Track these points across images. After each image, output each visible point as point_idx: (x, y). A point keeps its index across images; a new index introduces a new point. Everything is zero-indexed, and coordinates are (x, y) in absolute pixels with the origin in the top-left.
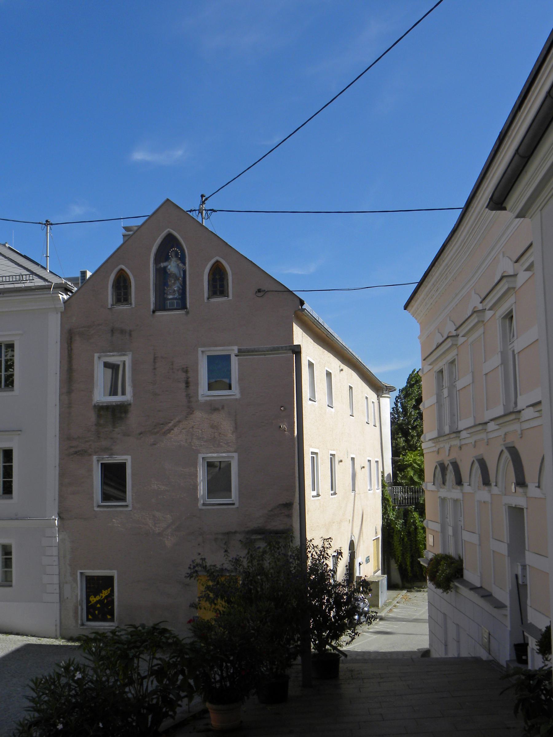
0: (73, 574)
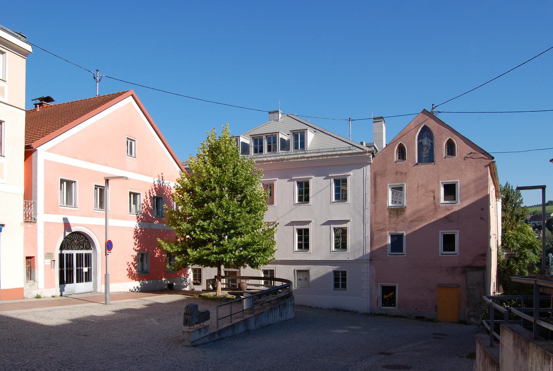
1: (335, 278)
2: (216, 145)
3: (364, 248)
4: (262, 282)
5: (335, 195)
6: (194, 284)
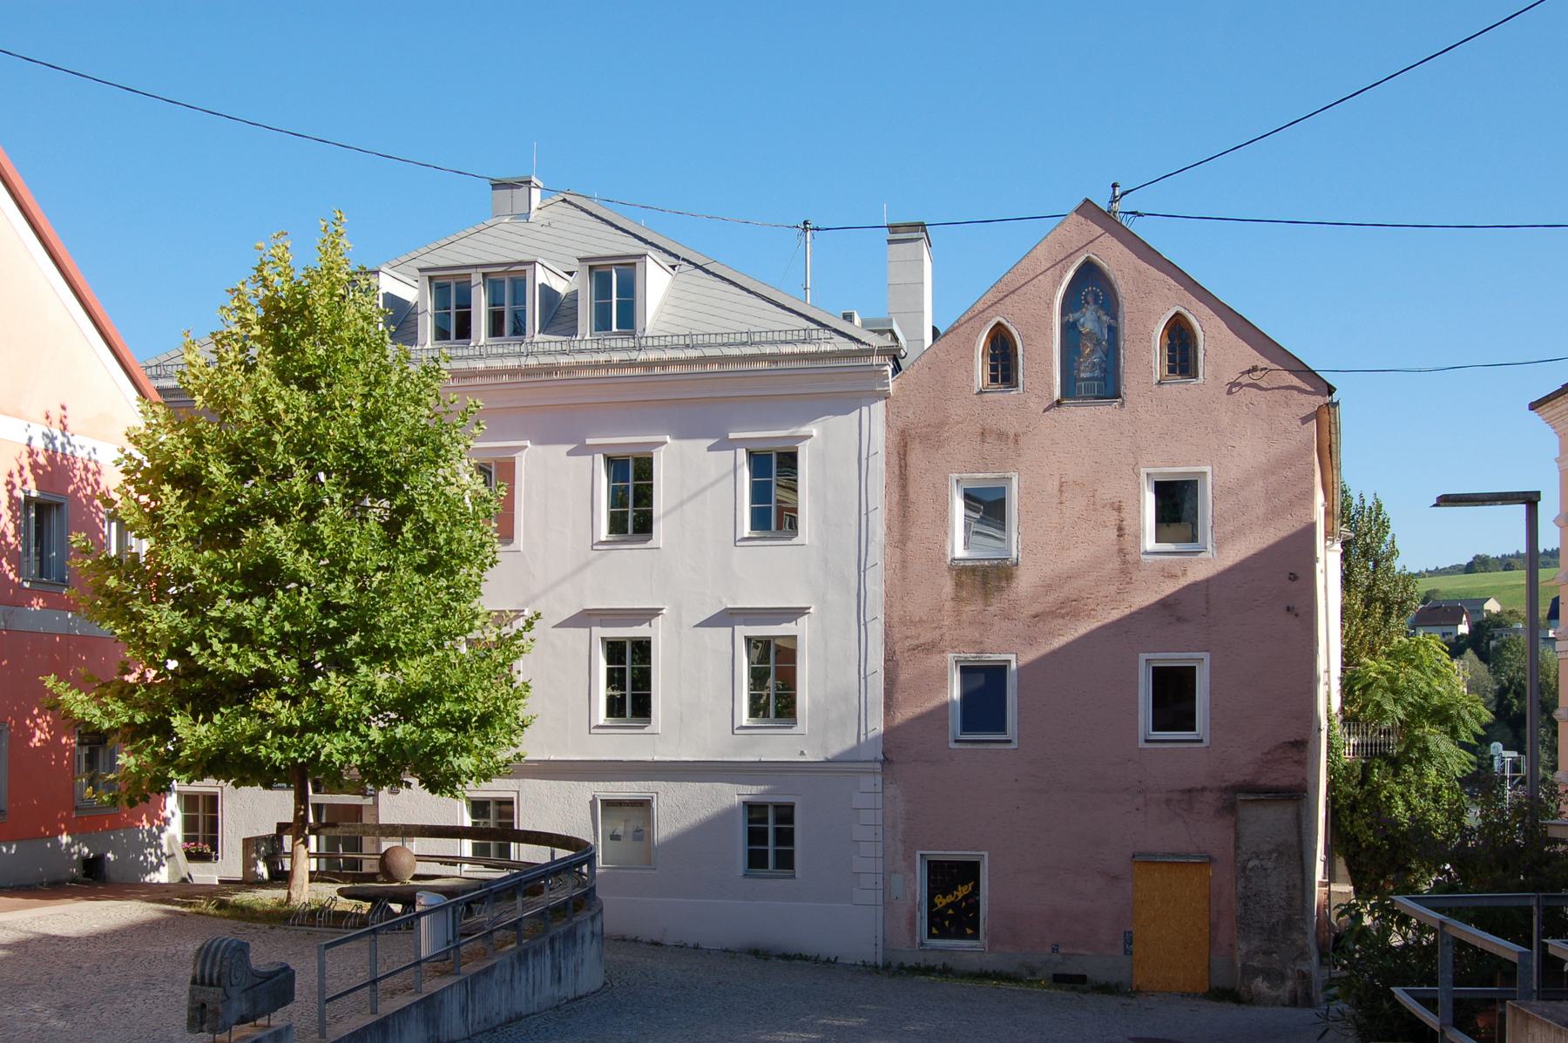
0: (908, 857)
1: (751, 831)
2: (295, 301)
3: (861, 717)
4: (467, 847)
5: (753, 511)
6: (192, 856)
